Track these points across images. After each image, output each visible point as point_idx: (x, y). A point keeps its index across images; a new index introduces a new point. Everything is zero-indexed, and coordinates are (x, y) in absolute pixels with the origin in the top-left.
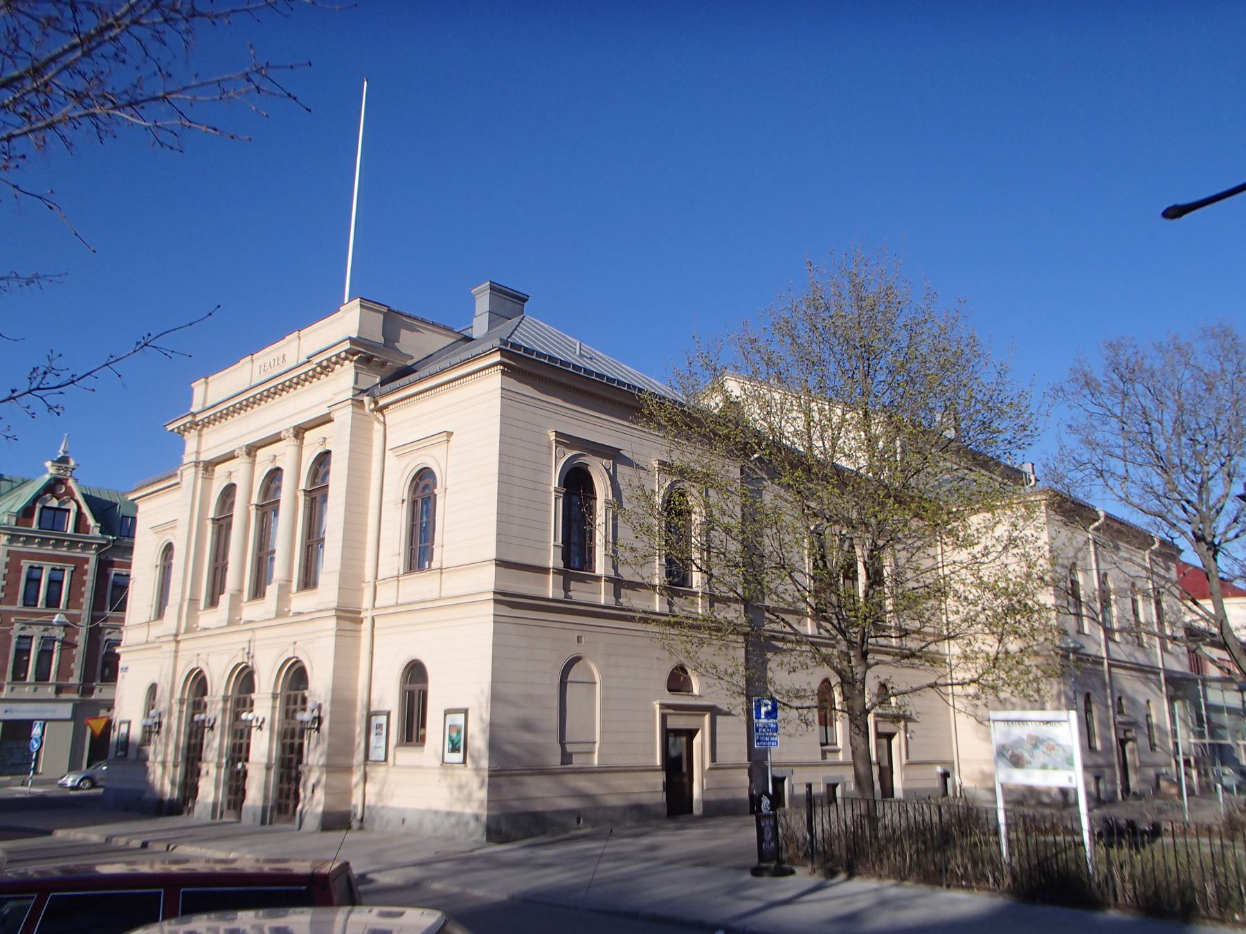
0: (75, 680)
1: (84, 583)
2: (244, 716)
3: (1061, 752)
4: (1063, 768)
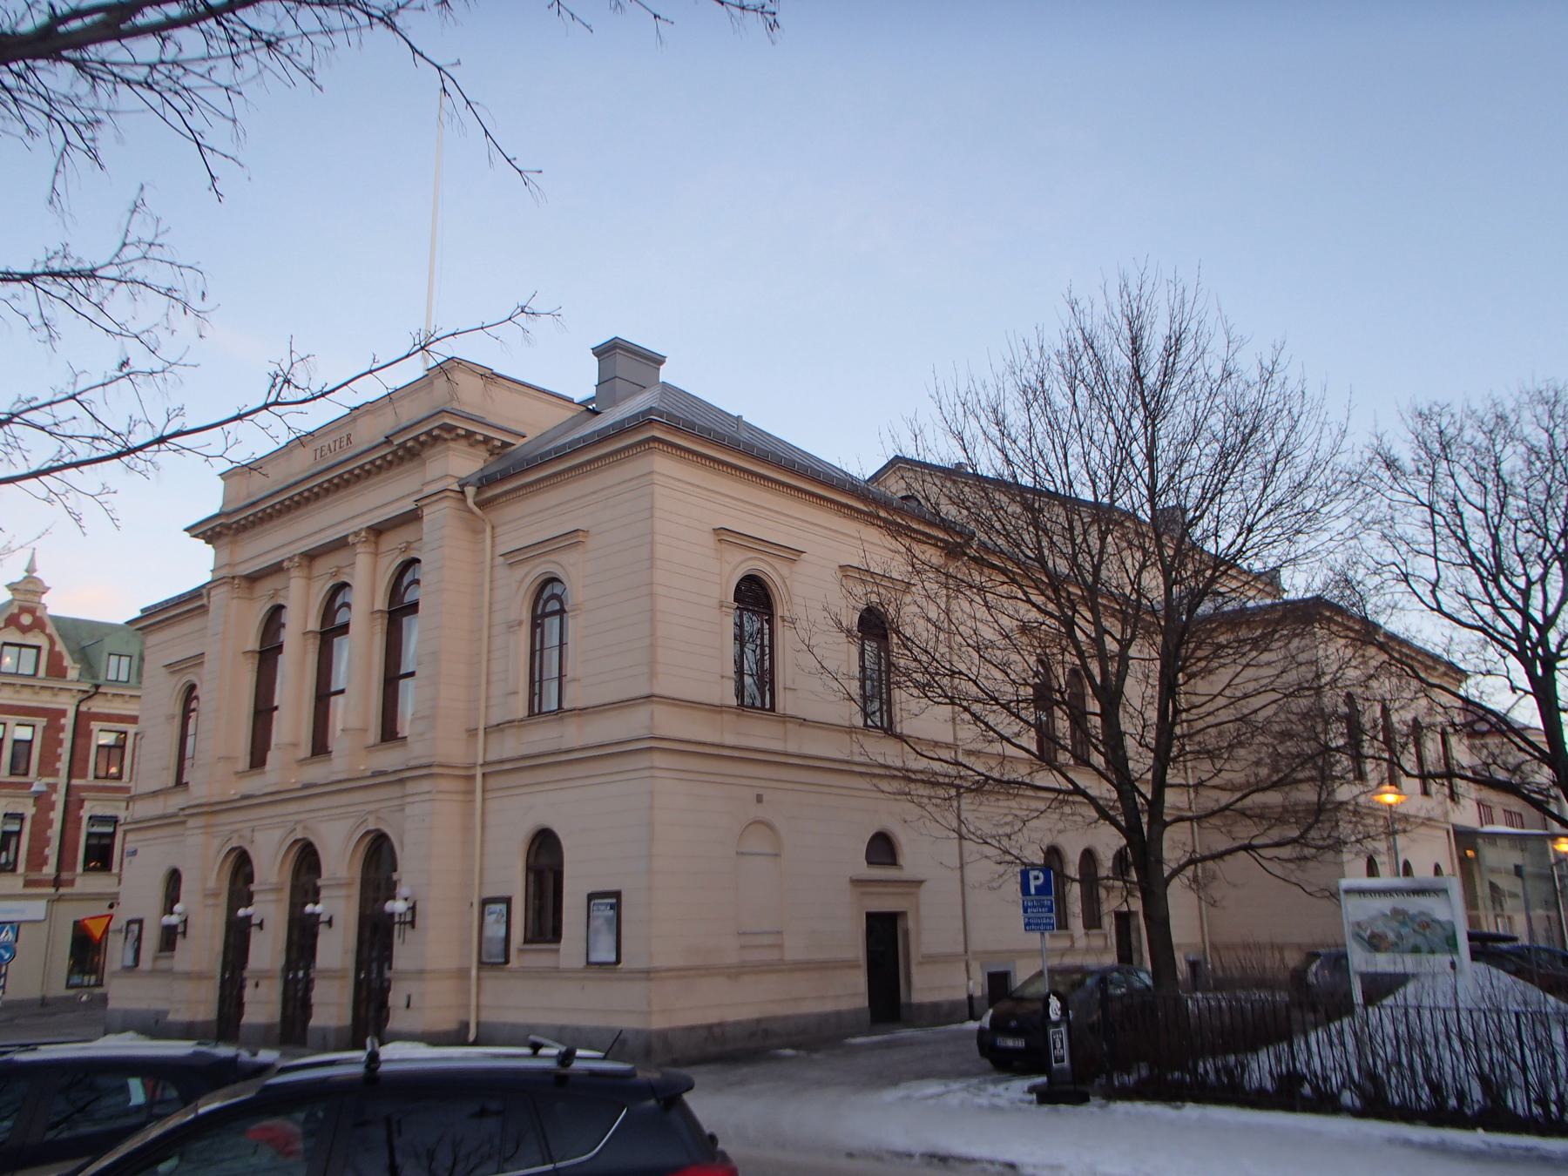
0: (49, 870)
1: (60, 743)
2: (309, 908)
3: (1439, 930)
4: (1443, 952)
